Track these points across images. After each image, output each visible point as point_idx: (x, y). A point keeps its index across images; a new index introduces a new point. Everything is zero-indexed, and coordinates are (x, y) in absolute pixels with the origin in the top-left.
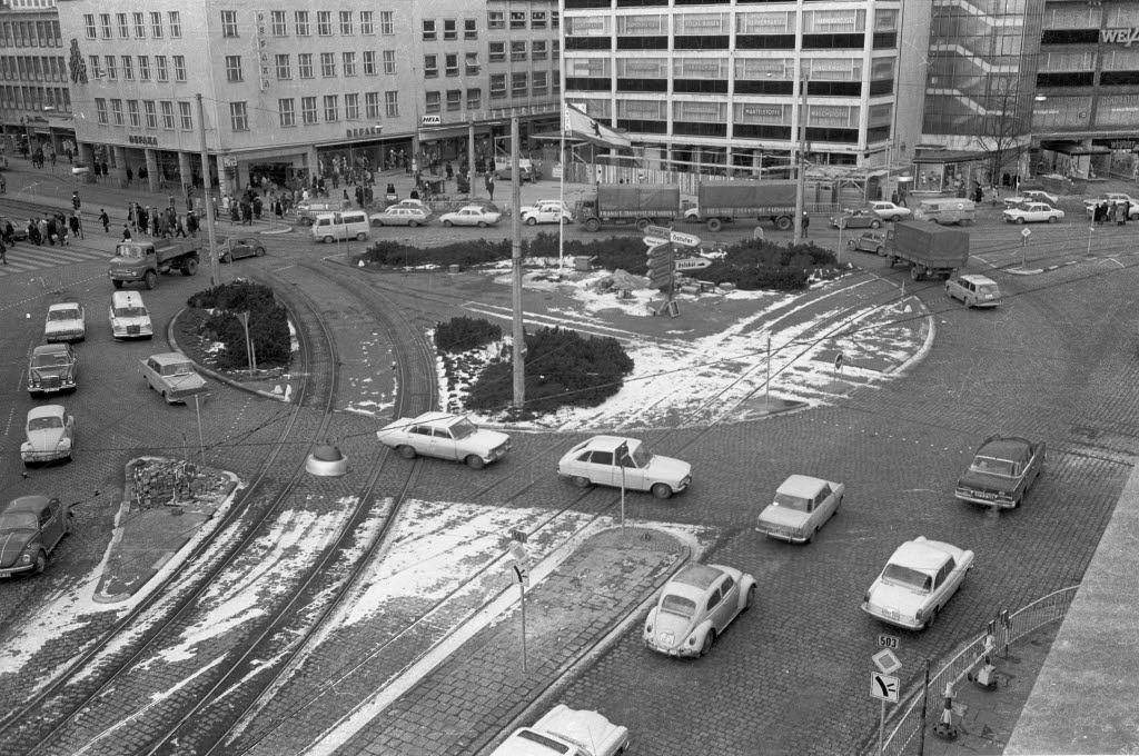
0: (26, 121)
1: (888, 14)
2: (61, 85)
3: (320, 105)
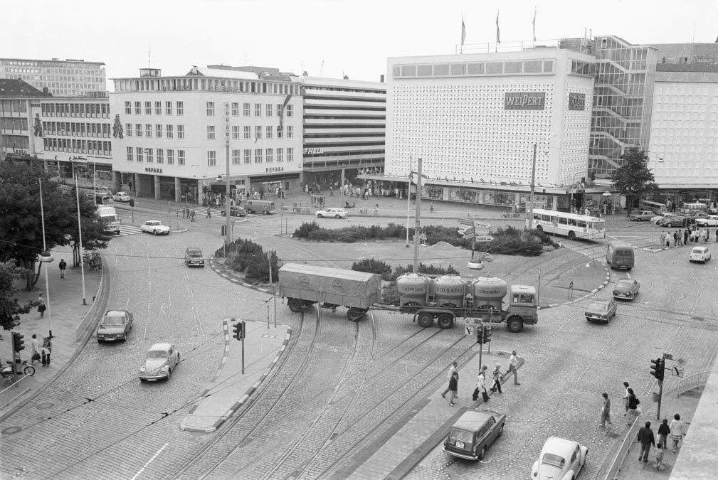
0: (73, 158)
1: (437, 189)
2: (107, 140)
3: (264, 154)
